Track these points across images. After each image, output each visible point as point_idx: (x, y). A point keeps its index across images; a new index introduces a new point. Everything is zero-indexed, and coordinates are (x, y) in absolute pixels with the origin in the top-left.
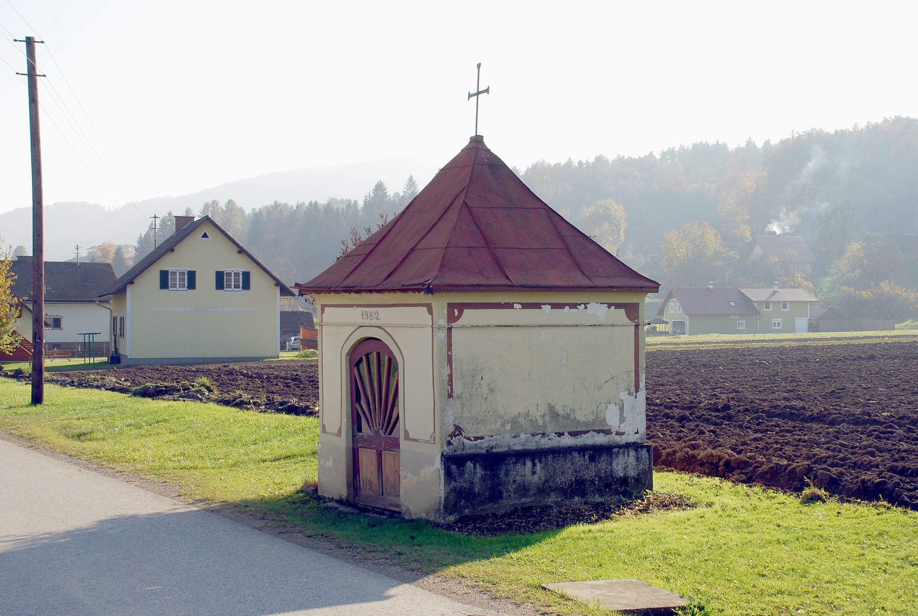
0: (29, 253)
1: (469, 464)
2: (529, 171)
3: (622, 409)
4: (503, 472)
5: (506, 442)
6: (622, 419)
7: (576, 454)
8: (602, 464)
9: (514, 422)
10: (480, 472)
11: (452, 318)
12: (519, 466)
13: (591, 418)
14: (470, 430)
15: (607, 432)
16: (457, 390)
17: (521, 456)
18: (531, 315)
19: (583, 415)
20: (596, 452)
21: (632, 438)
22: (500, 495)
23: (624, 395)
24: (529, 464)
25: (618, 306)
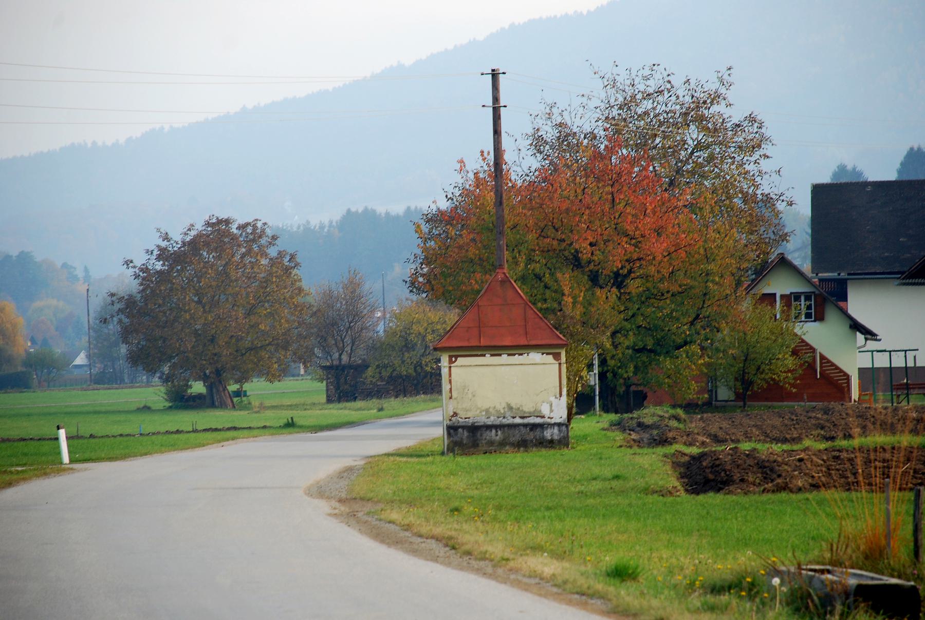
0: (491, 207)
1: (460, 430)
2: (900, 172)
3: (551, 406)
4: (479, 434)
5: (482, 420)
6: (551, 411)
7: (522, 428)
8: (538, 432)
9: (487, 411)
10: (466, 434)
11: (451, 362)
12: (488, 432)
13: (532, 410)
14: (462, 414)
15: (543, 417)
16: (454, 394)
17: (489, 427)
18: (496, 360)
19: (528, 408)
20: (534, 427)
21: (558, 421)
22: (478, 445)
23: (552, 399)
24: (494, 431)
25: (548, 354)
